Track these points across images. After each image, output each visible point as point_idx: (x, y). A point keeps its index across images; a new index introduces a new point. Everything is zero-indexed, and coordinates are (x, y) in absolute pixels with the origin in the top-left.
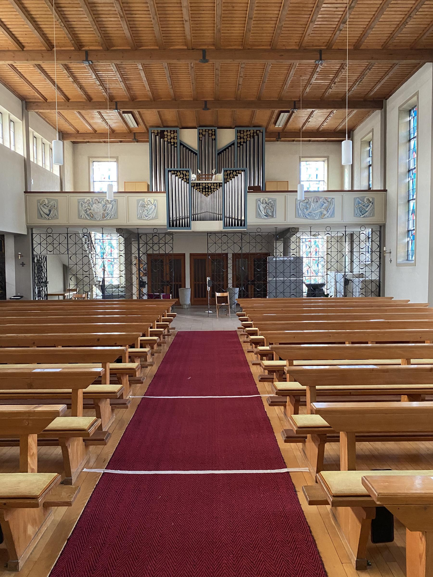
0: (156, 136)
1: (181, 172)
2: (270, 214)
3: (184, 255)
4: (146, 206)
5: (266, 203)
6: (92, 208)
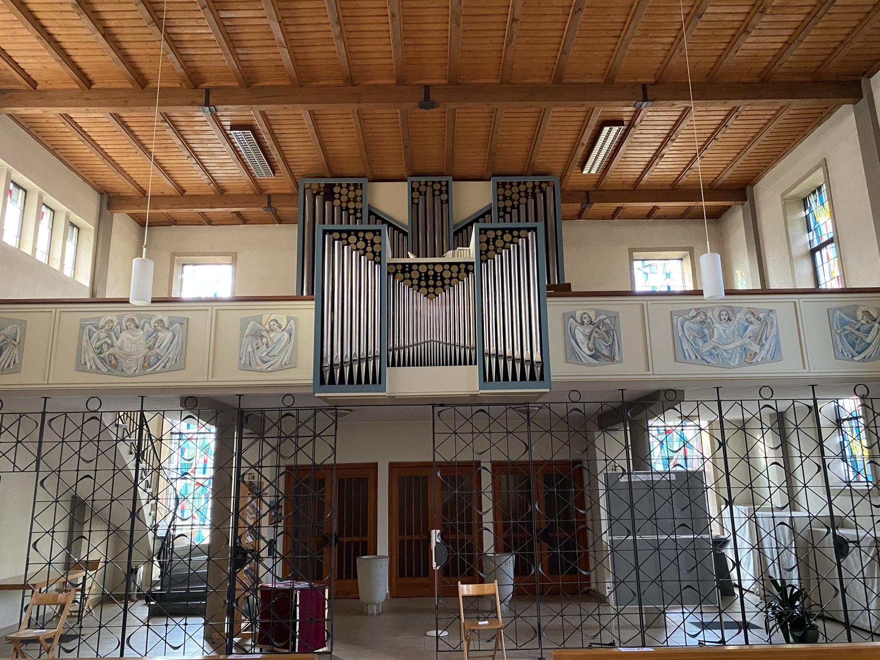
0: (314, 196)
1: (361, 235)
2: (606, 352)
3: (375, 465)
4: (264, 333)
5: (591, 323)
6: (117, 343)
